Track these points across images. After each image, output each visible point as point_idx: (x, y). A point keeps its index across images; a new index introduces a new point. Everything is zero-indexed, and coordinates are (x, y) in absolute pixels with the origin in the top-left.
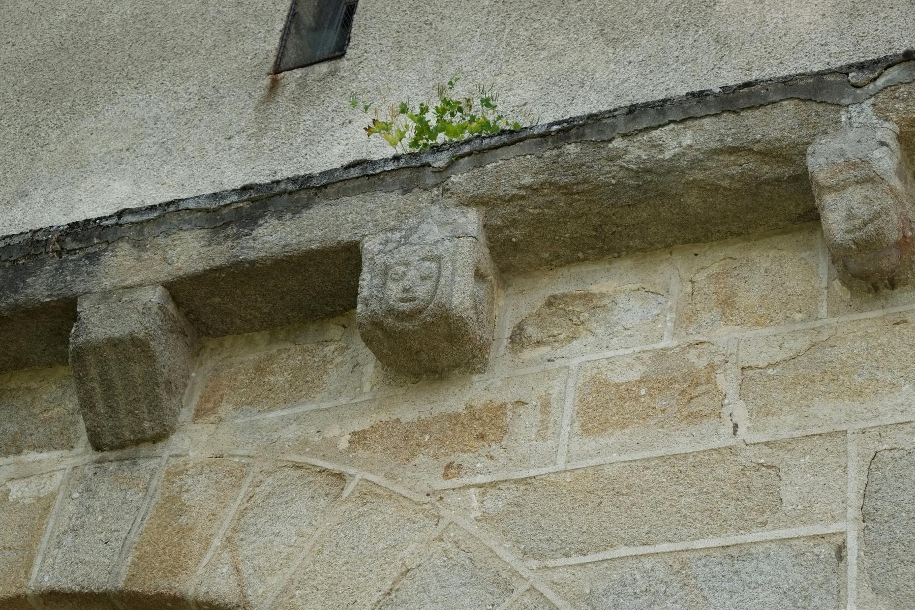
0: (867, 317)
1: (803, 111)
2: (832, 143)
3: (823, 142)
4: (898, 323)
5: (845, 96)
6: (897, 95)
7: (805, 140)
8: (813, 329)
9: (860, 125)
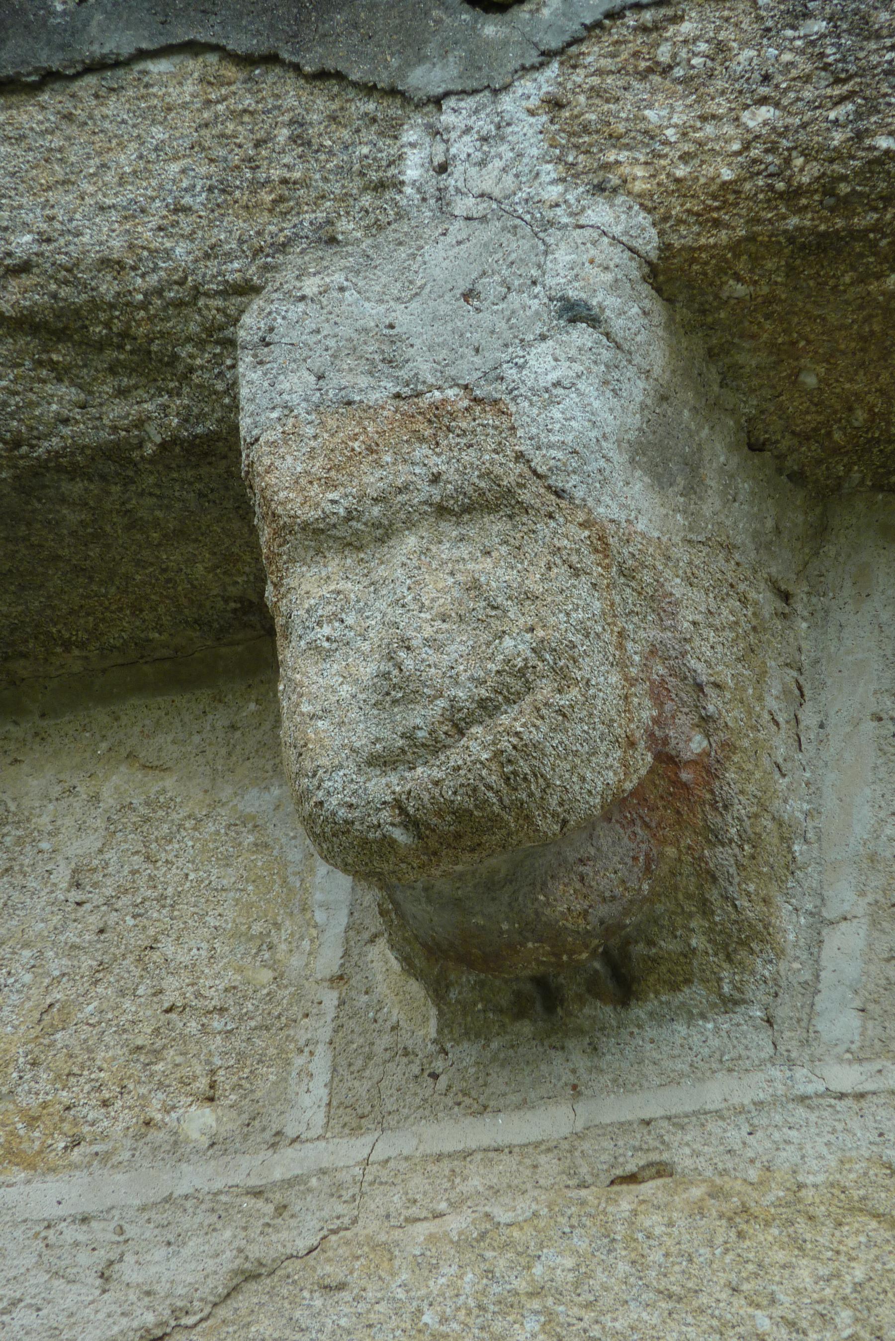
0: (502, 1140)
1: (237, 115)
2: (350, 296)
3: (310, 286)
4: (632, 1179)
5: (430, 49)
6: (664, 53)
7: (234, 270)
8: (257, 1193)
9: (483, 207)
